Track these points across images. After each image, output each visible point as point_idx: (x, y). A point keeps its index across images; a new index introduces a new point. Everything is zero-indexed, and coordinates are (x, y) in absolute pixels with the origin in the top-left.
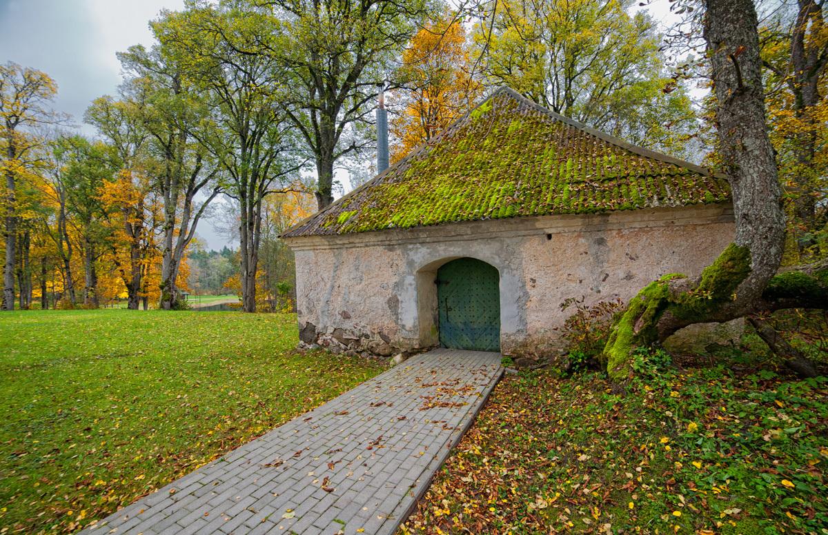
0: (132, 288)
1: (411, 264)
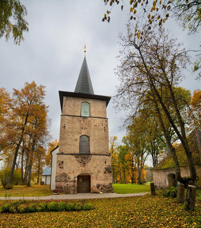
0: (132, 179)
1: (166, 174)
